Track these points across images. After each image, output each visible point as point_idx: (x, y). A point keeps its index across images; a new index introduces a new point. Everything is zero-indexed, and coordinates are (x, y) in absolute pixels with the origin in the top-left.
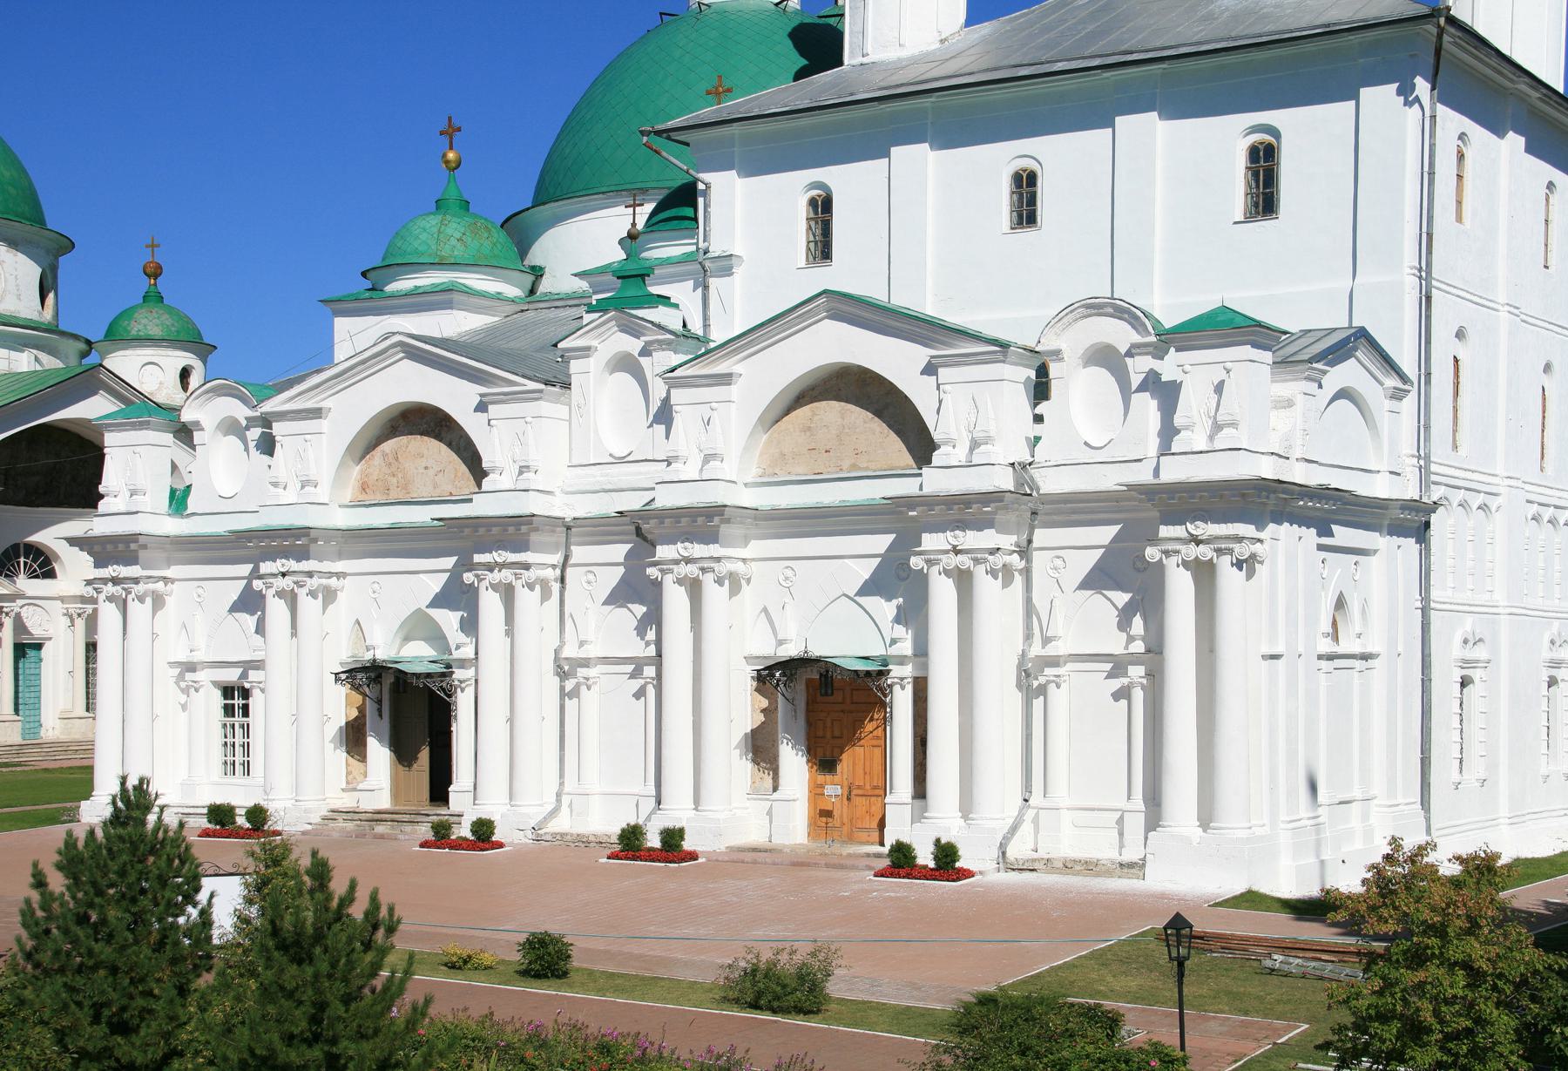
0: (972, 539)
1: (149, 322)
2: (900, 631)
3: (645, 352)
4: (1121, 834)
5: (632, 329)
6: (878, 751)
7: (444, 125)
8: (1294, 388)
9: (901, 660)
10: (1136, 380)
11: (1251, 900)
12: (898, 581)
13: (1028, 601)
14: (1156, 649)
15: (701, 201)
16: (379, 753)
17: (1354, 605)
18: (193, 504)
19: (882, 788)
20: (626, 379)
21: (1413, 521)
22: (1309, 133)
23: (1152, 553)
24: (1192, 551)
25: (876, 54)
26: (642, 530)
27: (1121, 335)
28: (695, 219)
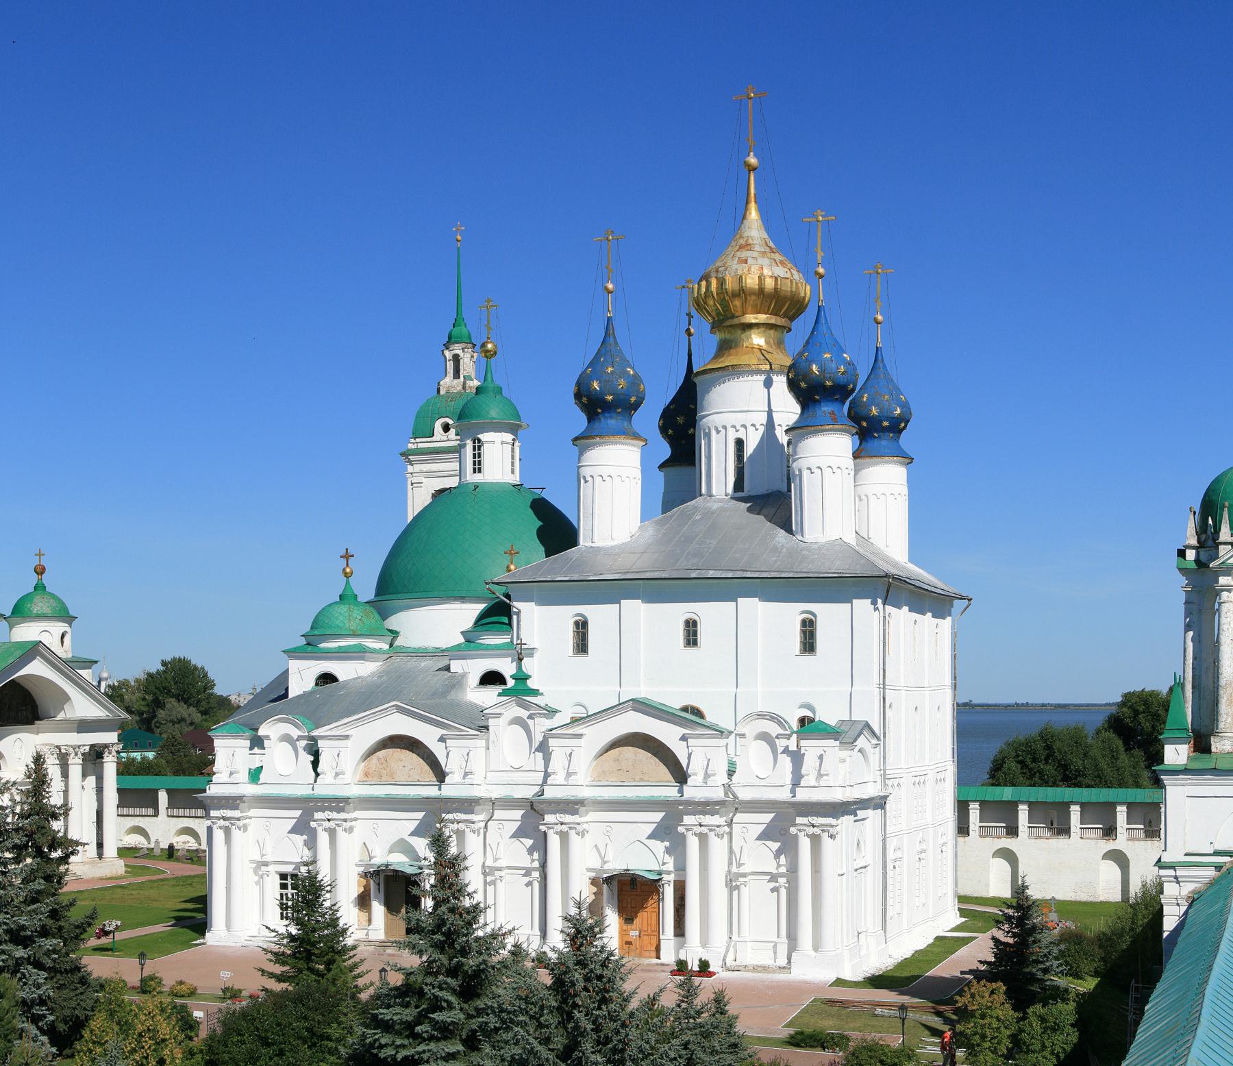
0: (708, 820)
1: (40, 606)
2: (668, 859)
3: (530, 717)
4: (775, 953)
5: (525, 705)
6: (654, 915)
7: (343, 553)
8: (845, 754)
9: (669, 873)
10: (780, 749)
11: (839, 982)
12: (669, 831)
13: (731, 848)
14: (793, 870)
15: (515, 617)
16: (378, 909)
17: (862, 843)
18: (263, 777)
19: (658, 932)
20: (518, 729)
21: (879, 803)
22: (830, 615)
23: (793, 830)
24: (811, 830)
25: (599, 543)
26: (535, 809)
27: (774, 729)
28: (510, 624)
